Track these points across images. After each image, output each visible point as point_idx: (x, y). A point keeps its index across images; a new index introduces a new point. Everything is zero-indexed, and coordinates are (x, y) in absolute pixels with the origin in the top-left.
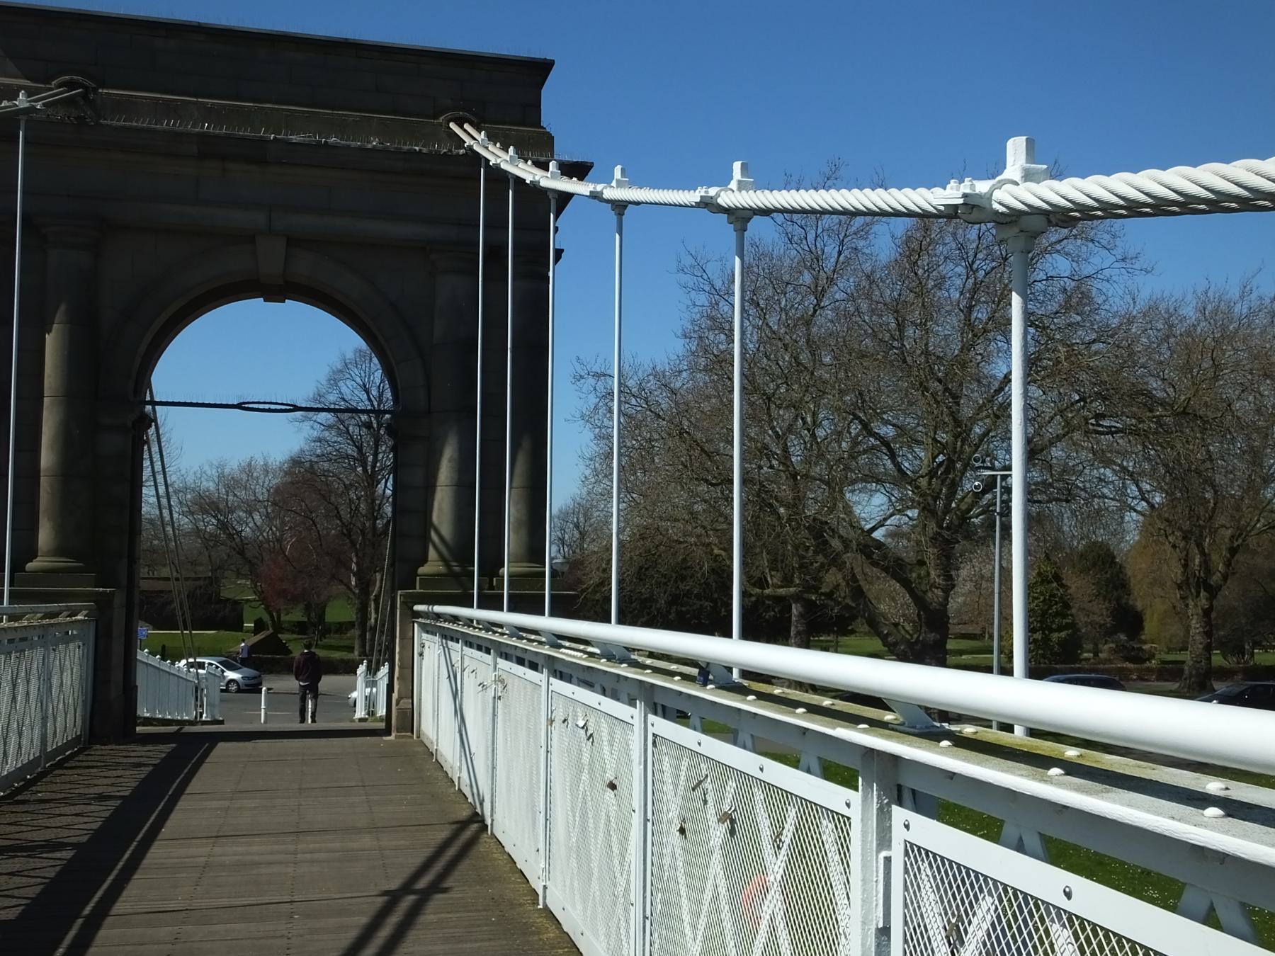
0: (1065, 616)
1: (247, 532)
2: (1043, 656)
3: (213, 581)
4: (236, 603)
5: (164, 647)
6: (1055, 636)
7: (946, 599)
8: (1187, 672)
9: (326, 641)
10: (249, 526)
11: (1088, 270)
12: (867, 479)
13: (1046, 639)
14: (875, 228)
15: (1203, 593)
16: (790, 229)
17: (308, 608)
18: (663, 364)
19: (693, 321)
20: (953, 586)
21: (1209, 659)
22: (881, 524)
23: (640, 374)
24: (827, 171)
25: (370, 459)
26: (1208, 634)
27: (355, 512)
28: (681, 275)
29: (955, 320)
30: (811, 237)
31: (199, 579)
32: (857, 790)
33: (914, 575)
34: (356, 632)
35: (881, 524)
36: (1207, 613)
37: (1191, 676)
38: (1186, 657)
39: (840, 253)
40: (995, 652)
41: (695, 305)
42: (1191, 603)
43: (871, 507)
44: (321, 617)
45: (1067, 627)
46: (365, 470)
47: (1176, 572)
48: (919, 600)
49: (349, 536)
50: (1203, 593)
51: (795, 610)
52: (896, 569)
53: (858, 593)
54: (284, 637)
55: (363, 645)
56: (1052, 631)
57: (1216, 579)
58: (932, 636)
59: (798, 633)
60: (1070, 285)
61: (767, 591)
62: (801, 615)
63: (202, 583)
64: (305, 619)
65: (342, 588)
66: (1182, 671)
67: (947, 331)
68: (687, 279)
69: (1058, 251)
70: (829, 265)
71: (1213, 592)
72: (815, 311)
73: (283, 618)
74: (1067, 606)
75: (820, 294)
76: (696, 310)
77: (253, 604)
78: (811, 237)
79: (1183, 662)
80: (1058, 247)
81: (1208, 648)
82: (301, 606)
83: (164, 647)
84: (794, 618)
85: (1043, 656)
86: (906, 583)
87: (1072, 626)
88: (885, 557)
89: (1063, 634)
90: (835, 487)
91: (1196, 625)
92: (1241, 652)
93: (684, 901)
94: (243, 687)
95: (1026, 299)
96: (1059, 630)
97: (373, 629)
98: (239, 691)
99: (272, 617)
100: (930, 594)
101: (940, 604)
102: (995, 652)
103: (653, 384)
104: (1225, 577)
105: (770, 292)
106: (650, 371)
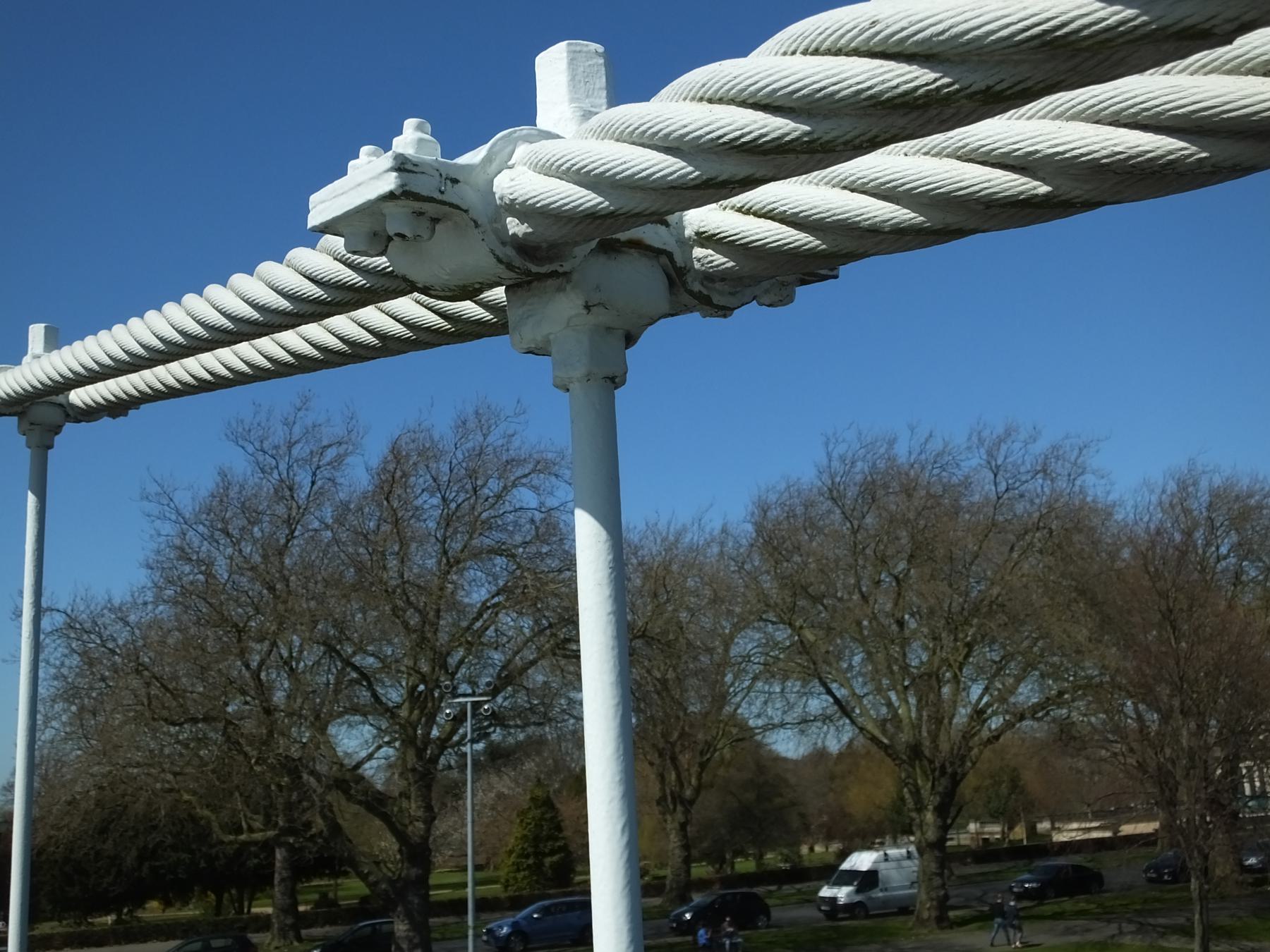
0: (557, 839)
2: (537, 882)
6: (548, 861)
7: (428, 830)
8: (668, 887)
11: (551, 502)
12: (355, 710)
13: (539, 866)
14: (349, 460)
15: (679, 808)
16: (261, 459)
18: (120, 595)
19: (158, 552)
20: (434, 818)
21: (688, 872)
22: (370, 757)
23: (92, 608)
24: (298, 404)
26: (686, 847)
28: (145, 503)
29: (433, 548)
30: (283, 466)
33: (396, 809)
35: (370, 757)
36: (683, 827)
37: (672, 889)
38: (667, 872)
39: (313, 483)
40: (470, 885)
41: (159, 535)
42: (669, 818)
43: (353, 740)
45: (561, 849)
46: (486, 702)
47: (655, 790)
48: (401, 836)
50: (679, 808)
51: (279, 854)
52: (376, 803)
53: (336, 829)
56: (545, 855)
57: (688, 793)
58: (414, 872)
59: (283, 880)
60: (538, 516)
61: (243, 837)
62: (285, 860)
66: (664, 885)
67: (425, 560)
68: (153, 508)
69: (524, 485)
70: (302, 495)
71: (688, 804)
72: (288, 541)
74: (559, 828)
75: (290, 522)
76: (162, 539)
78: (283, 466)
79: (665, 877)
80: (524, 481)
81: (687, 861)
84: (278, 864)
85: (537, 882)
86: (386, 818)
87: (564, 849)
88: (365, 793)
89: (555, 858)
90: (321, 724)
91: (674, 840)
92: (722, 861)
95: (611, 520)
96: (552, 853)
100: (410, 828)
101: (422, 837)
102: (470, 885)
103: (109, 617)
104: (698, 790)
105: (242, 522)
106: (103, 603)
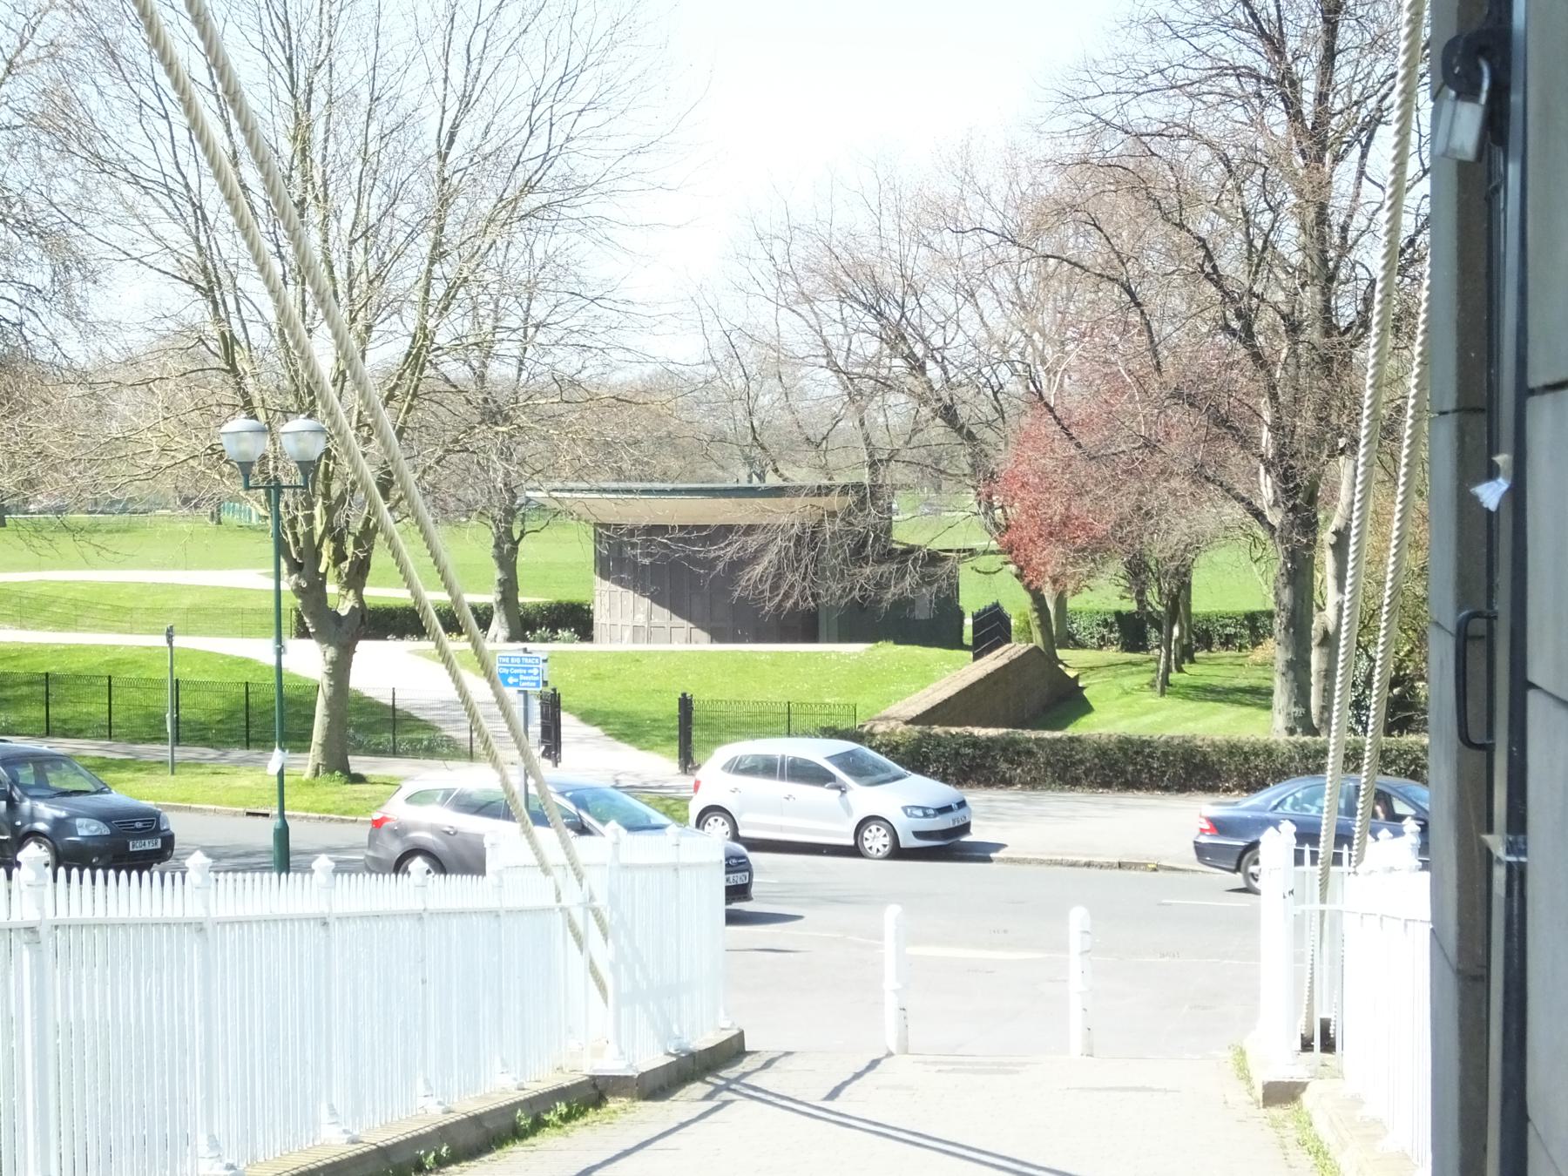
1: (959, 349)
3: (868, 496)
4: (934, 558)
5: (686, 704)
9: (1193, 673)
10: (972, 330)
17: (1137, 571)
25: (1310, 86)
27: (1260, 256)
31: (829, 490)
32: (829, 758)
34: (1273, 651)
44: (1178, 600)
46: (1295, 115)
49: (1248, 335)
54: (1072, 660)
55: (1301, 694)
63: (834, 502)
64: (1132, 606)
65: (1234, 512)
73: (1072, 603)
77: (983, 562)
82: (1117, 567)
83: (686, 704)
93: (992, 732)
94: (907, 841)
97: (1329, 640)
98: (898, 853)
99: (1038, 599)
